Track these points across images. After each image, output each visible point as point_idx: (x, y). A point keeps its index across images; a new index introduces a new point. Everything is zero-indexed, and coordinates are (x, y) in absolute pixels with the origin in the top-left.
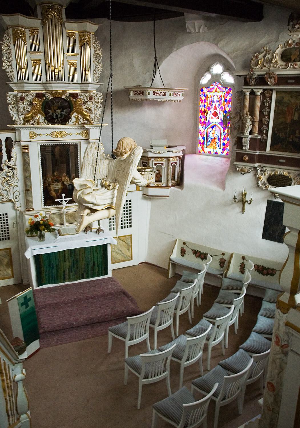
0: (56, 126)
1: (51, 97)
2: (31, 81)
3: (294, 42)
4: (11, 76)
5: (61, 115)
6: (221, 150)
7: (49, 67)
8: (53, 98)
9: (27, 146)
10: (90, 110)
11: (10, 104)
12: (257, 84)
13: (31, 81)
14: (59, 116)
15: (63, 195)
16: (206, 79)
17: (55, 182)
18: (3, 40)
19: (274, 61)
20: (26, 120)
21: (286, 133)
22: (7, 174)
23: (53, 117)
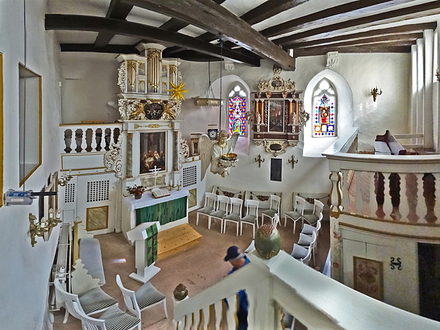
0: (152, 120)
1: (151, 103)
2: (137, 92)
3: (277, 78)
4: (123, 89)
5: (156, 114)
6: (241, 133)
7: (150, 84)
8: (152, 103)
9: (132, 134)
10: (174, 111)
11: (120, 106)
12: (261, 97)
13: (137, 92)
14: (155, 114)
15: (155, 167)
16: (231, 94)
17: (149, 157)
18: (121, 68)
19: (269, 86)
20: (132, 117)
21: (276, 122)
22: (113, 152)
23: (151, 115)
